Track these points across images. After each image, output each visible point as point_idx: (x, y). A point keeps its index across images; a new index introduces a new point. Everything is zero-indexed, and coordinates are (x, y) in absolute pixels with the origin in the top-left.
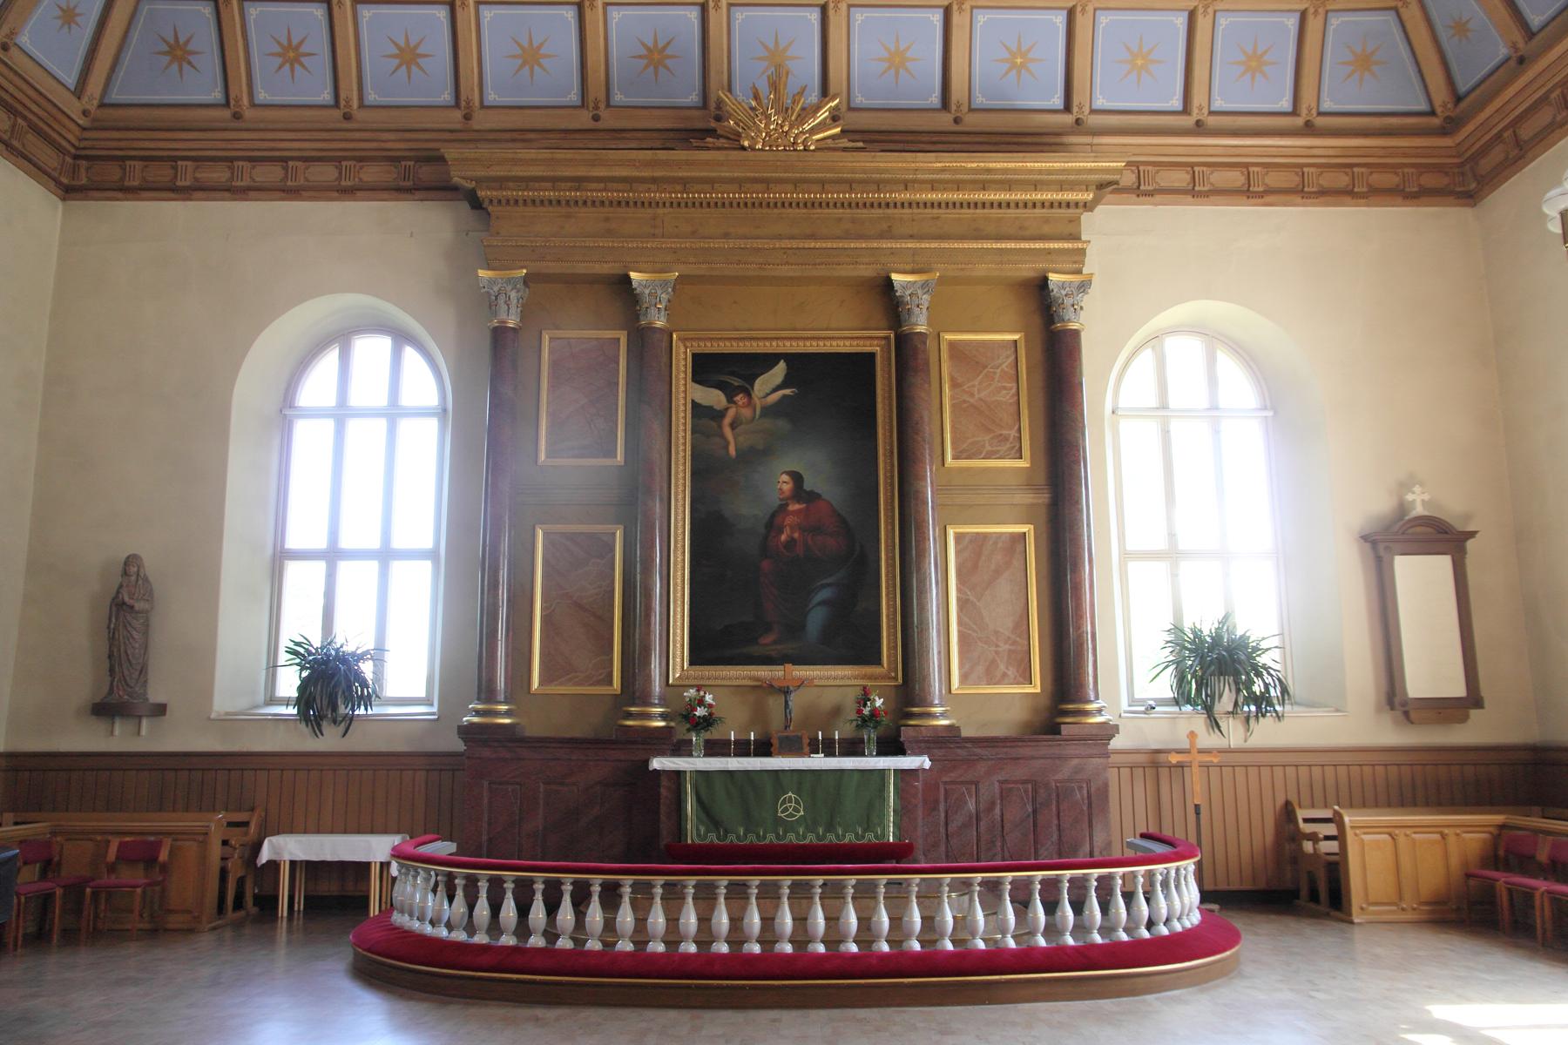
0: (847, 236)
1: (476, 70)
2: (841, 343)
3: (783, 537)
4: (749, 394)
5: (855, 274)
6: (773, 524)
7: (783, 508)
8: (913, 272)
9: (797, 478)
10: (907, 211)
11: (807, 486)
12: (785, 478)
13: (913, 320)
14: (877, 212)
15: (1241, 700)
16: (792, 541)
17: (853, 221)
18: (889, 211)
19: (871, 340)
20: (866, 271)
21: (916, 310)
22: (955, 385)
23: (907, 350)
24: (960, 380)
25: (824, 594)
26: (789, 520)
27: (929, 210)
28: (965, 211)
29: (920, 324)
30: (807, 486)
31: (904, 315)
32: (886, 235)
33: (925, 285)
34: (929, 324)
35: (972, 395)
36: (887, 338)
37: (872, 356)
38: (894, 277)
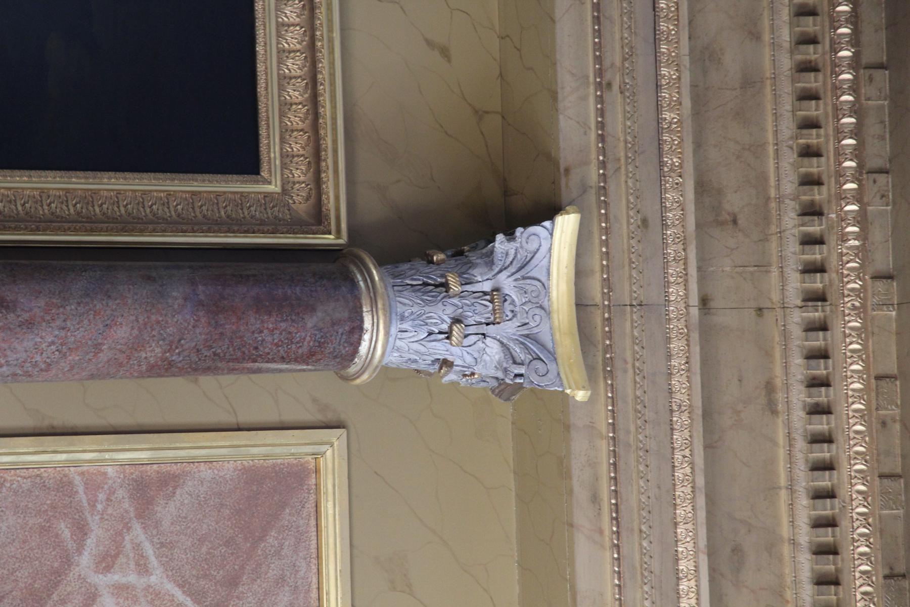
0: (704, 57)
1: (178, 445)
2: (294, 39)
5: (566, 82)
8: (581, 305)
10: (795, 284)
13: (408, 304)
14: (783, 170)
15: (343, 341)
17: (750, 83)
18: (791, 221)
19: (295, 170)
20: (574, 126)
21: (441, 314)
22: (147, 489)
23: (293, 283)
24: (167, 511)
27: (799, 368)
28: (805, 509)
29: (392, 334)
31: (418, 273)
32: (713, 214)
33: (536, 347)
34: (387, 373)
35: (106, 562)
36: (318, 218)
37: (250, 165)
38: (566, 225)
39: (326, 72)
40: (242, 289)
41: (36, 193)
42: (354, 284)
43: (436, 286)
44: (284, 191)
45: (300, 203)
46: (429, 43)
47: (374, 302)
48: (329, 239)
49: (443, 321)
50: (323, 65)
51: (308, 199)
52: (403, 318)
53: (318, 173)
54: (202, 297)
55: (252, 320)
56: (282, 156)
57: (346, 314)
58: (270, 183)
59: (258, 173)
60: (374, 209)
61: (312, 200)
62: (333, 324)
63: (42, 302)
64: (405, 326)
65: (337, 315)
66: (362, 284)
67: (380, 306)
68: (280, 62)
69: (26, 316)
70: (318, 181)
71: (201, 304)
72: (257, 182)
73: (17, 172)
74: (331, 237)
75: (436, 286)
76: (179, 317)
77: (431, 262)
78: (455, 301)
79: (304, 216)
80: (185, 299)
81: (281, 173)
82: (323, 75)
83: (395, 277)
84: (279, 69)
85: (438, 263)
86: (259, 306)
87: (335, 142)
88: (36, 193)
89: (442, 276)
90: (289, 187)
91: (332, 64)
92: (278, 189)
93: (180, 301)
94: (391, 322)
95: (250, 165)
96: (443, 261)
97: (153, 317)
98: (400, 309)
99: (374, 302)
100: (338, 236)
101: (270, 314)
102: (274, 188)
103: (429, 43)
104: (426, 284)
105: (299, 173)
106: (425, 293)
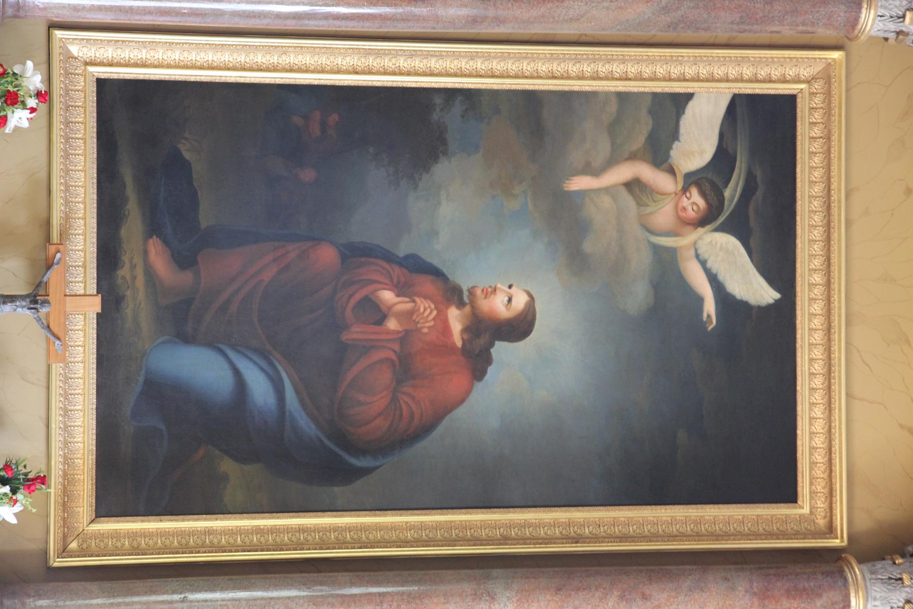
3: (387, 296)
4: (703, 221)
6: (419, 271)
7: (453, 295)
9: (519, 327)
11: (501, 350)
12: (520, 301)
13: (878, 590)
16: (379, 315)
25: (260, 388)
26: (426, 309)
30: (501, 350)
31: (885, 568)
36: (830, 530)
37: (791, 497)
39: (837, 447)
40: (779, 584)
41: (669, 519)
42: (846, 579)
43: (896, 580)
44: (811, 513)
45: (821, 522)
46: (901, 426)
47: (857, 592)
48: (836, 543)
49: (900, 601)
50: (836, 443)
51: (825, 517)
52: (875, 599)
53: (831, 503)
54: (755, 590)
55: (784, 602)
56: (810, 493)
57: (841, 598)
58: (803, 508)
59: (796, 502)
60: (864, 523)
61: (828, 519)
62: (833, 604)
63: (665, 595)
64: (877, 603)
65: (835, 599)
66: (850, 579)
67: (861, 594)
68: (811, 439)
69: (657, 603)
70: (831, 508)
71: (755, 594)
72: (795, 508)
73: (659, 507)
74: (838, 541)
75: (896, 580)
76: (742, 602)
77: (895, 563)
78: (908, 589)
79: (823, 529)
80: (746, 591)
81: (809, 501)
82: (836, 448)
83: (872, 573)
84: (810, 443)
85: (899, 565)
86: (788, 594)
87: (841, 486)
88: (669, 519)
89: (900, 574)
90: (814, 510)
91: (841, 443)
92: (808, 512)
93: (743, 593)
94: (867, 600)
95: (791, 497)
96: (902, 564)
97: (727, 603)
98: (874, 594)
99: (857, 592)
100: (842, 541)
101: (795, 599)
102: (806, 510)
103: (901, 426)
104: (890, 578)
105: (821, 504)
106: (889, 584)
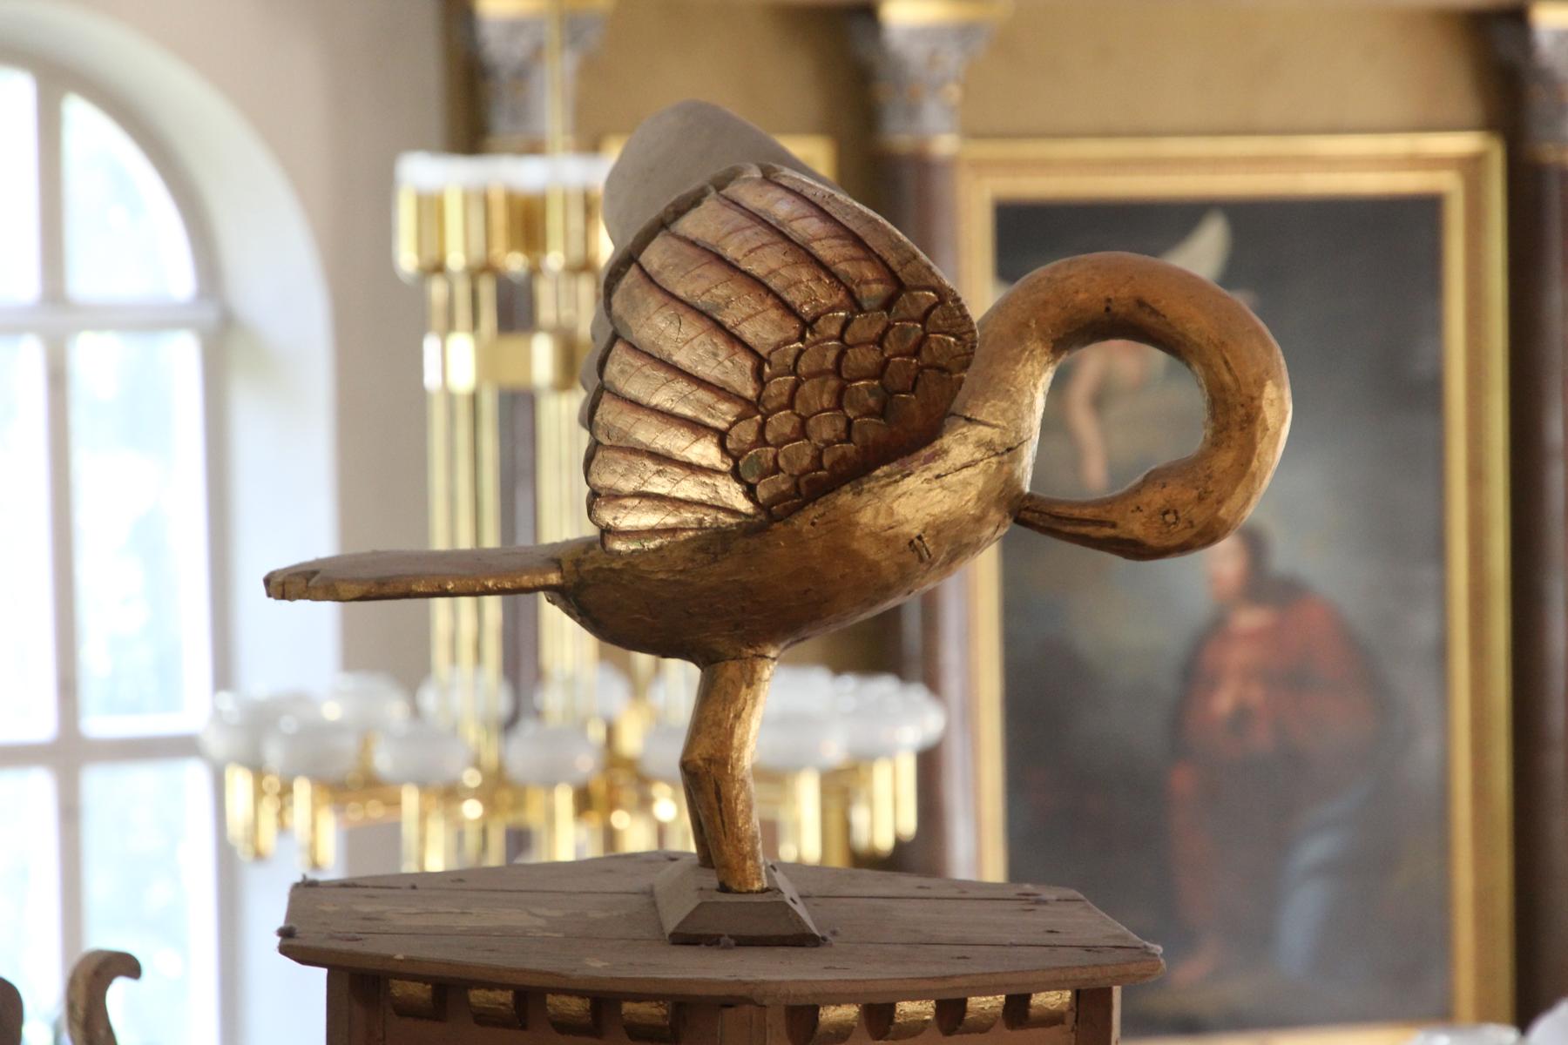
6: (1194, 673)
7: (1215, 629)
37: (1428, 208)
